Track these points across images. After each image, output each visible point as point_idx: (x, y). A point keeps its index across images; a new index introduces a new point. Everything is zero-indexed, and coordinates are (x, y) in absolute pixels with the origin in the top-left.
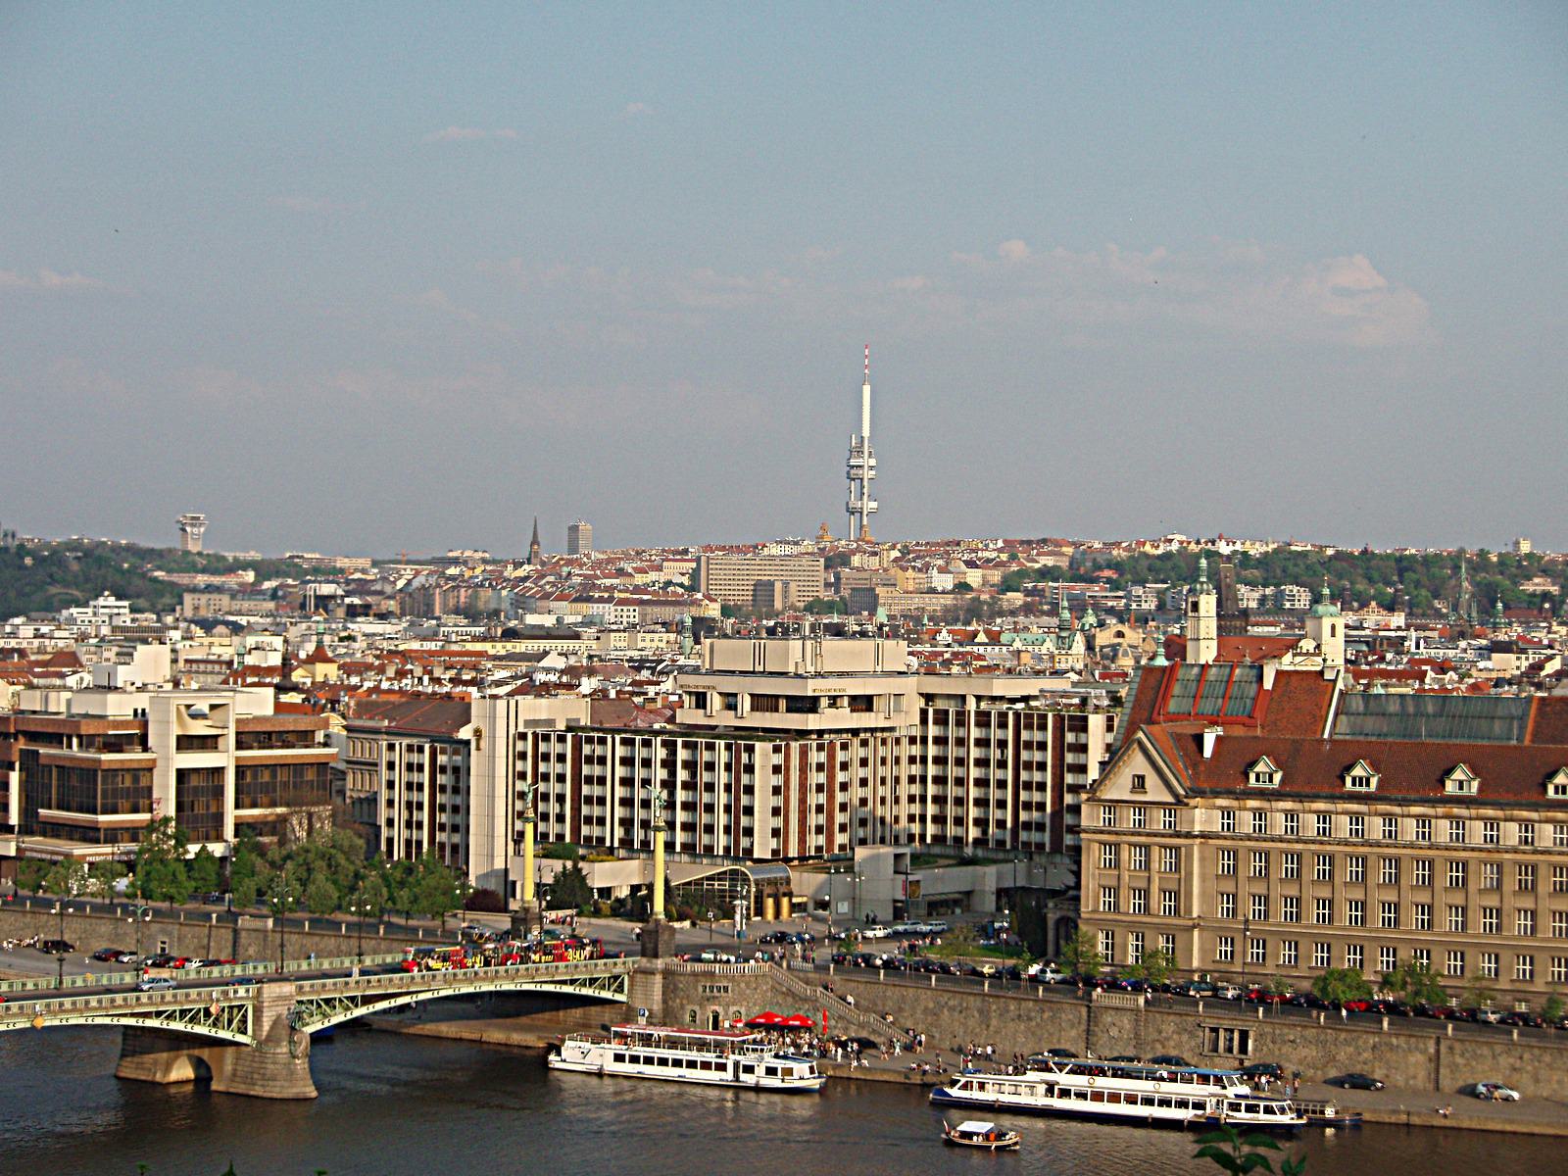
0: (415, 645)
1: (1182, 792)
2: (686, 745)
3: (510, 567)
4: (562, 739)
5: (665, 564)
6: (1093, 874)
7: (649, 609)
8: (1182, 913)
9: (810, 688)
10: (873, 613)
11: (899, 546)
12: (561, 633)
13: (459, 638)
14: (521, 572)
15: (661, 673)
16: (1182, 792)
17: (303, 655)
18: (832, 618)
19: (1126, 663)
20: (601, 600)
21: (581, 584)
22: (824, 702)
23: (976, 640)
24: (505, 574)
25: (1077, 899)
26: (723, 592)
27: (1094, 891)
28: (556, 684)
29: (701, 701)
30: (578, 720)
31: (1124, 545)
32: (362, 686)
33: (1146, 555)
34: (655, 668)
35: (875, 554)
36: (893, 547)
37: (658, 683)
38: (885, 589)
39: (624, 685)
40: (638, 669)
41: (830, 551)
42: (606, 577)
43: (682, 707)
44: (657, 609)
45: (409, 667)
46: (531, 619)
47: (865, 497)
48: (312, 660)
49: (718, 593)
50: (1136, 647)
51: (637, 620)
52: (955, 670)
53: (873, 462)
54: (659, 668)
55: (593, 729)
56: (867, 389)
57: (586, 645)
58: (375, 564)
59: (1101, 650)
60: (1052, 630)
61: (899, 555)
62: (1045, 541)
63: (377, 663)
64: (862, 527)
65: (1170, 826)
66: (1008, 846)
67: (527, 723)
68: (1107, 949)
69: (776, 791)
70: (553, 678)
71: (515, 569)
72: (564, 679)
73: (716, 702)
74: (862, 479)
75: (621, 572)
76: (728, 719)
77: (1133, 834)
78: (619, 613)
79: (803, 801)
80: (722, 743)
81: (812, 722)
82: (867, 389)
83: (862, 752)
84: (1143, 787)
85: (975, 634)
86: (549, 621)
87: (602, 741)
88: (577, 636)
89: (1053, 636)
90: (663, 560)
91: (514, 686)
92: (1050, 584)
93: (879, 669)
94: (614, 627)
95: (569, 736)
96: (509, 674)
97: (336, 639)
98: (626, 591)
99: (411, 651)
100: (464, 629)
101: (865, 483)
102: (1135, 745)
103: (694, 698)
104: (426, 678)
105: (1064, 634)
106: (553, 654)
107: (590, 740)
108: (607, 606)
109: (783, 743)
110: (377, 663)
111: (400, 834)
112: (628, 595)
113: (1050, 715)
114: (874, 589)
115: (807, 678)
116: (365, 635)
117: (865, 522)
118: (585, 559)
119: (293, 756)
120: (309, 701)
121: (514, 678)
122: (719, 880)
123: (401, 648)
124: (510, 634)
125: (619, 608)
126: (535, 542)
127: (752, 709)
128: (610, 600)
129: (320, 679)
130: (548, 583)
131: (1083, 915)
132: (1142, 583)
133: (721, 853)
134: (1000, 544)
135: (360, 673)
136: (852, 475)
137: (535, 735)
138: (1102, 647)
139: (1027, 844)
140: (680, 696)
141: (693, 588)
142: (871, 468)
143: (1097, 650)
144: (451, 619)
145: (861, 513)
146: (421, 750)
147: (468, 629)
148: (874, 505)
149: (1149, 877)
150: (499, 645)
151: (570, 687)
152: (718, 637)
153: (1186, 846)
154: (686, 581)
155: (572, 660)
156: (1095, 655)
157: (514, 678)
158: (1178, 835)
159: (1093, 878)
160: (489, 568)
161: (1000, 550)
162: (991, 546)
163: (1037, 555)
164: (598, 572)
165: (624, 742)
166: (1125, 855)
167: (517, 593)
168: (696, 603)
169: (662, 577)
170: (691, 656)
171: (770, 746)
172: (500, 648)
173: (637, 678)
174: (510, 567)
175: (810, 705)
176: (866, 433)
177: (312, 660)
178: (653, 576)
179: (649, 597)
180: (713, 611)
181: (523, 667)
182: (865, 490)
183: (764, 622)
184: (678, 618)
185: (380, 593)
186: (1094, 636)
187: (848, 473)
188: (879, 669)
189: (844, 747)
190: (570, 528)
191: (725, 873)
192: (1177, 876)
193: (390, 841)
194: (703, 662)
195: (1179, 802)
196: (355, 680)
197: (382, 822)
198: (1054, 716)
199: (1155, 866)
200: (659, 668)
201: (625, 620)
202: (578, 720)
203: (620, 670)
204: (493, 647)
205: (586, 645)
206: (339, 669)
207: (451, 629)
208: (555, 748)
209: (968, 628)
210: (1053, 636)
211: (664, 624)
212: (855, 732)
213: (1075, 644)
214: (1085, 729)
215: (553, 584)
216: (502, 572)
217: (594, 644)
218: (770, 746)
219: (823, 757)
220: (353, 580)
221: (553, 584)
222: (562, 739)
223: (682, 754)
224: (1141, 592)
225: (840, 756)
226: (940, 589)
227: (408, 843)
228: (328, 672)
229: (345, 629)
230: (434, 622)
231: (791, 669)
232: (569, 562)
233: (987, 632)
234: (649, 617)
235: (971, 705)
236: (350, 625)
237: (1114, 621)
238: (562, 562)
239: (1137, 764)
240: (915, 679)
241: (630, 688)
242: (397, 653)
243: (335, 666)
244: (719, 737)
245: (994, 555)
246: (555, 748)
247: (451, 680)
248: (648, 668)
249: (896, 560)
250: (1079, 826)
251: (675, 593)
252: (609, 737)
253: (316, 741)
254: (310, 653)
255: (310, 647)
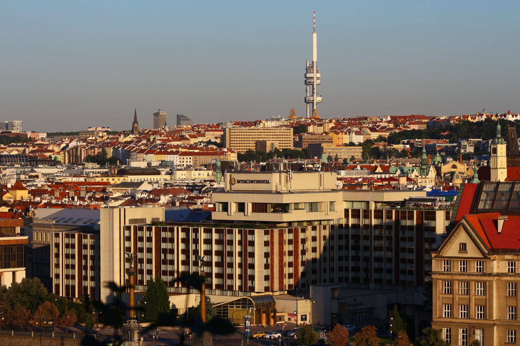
0: (70, 179)
1: (486, 252)
2: (216, 232)
3: (122, 136)
4: (149, 229)
5: (207, 133)
6: (439, 297)
7: (198, 157)
8: (488, 318)
9: (286, 199)
10: (320, 157)
11: (334, 121)
12: (150, 171)
13: (94, 175)
14: (128, 139)
15: (204, 192)
16: (486, 252)
17: (9, 186)
18: (298, 160)
19: (458, 182)
20: (172, 153)
21: (160, 145)
22: (292, 207)
23: (376, 171)
24: (119, 140)
25: (431, 311)
26: (238, 148)
27: (440, 305)
28: (146, 199)
29: (225, 207)
30: (159, 219)
31: (457, 118)
32: (41, 202)
33: (468, 121)
34: (201, 189)
35: (321, 125)
36: (331, 121)
37: (202, 198)
38: (327, 144)
39: (184, 199)
40: (192, 191)
41: (296, 124)
42: (174, 140)
43: (215, 211)
44: (202, 157)
45: (67, 191)
46: (134, 164)
47: (315, 95)
48: (14, 188)
49: (236, 148)
50: (463, 174)
51: (191, 164)
52: (364, 188)
53: (319, 75)
54: (203, 190)
55: (167, 224)
56: (315, 35)
57: (163, 178)
58: (49, 135)
59: (444, 175)
60: (417, 165)
61: (334, 125)
62: (413, 117)
63: (49, 189)
64: (313, 110)
65: (480, 271)
66: (393, 283)
67: (132, 221)
68: (447, 338)
69: (266, 244)
70: (145, 196)
71: (125, 137)
72: (151, 196)
73: (233, 208)
74: (313, 85)
75: (182, 138)
76: (240, 217)
77: (460, 275)
78: (181, 160)
79: (281, 260)
80: (237, 230)
81: (286, 217)
82: (315, 35)
83: (313, 233)
84: (465, 249)
85: (376, 167)
86: (143, 165)
87: (172, 230)
88: (158, 173)
89: (418, 168)
90: (206, 131)
91: (124, 201)
92: (417, 140)
93: (321, 188)
94: (179, 168)
95: (154, 227)
96: (121, 194)
97: (27, 177)
98: (185, 147)
99: (68, 183)
100: (97, 170)
101: (315, 87)
102: (461, 227)
103: (221, 205)
104: (76, 198)
105: (424, 167)
106: (146, 183)
107: (165, 230)
108: (175, 156)
109: (270, 229)
110: (49, 189)
111: (62, 282)
112: (186, 150)
113: (415, 212)
114: (320, 145)
115: (282, 194)
116: (44, 175)
117: (315, 108)
118: (163, 131)
119: (3, 241)
120: (13, 211)
121: (124, 196)
122: (236, 304)
123: (63, 181)
124: (122, 173)
125: (182, 157)
126: (135, 122)
127: (253, 211)
128: (177, 153)
129: (18, 198)
130: (143, 144)
131: (434, 320)
132: (467, 138)
133: (237, 289)
134: (389, 119)
135: (40, 195)
136: (308, 82)
137: (135, 227)
138: (445, 174)
139: (404, 282)
140: (214, 205)
141: (221, 145)
142: (318, 78)
143: (442, 175)
144: (90, 165)
145: (313, 103)
146: (73, 236)
147: (99, 170)
148: (319, 99)
149: (469, 298)
150: (116, 179)
151: (154, 201)
152: (233, 172)
153: (489, 281)
154: (218, 141)
155: (156, 186)
156: (441, 178)
157: (124, 196)
158: (485, 275)
159: (439, 300)
160: (111, 136)
161: (389, 122)
162: (384, 120)
163: (409, 124)
164: (170, 138)
165: (183, 230)
166: (456, 287)
167: (126, 150)
168: (223, 153)
169: (205, 139)
170: (221, 183)
171: (262, 231)
172: (118, 180)
173: (191, 195)
174: (122, 136)
175: (284, 208)
176: (315, 59)
177: (14, 188)
178: (200, 139)
179: (198, 151)
180: (233, 157)
181: (129, 190)
182: (315, 91)
183: (261, 163)
184: (213, 162)
185: (52, 151)
186: (440, 167)
187: (306, 81)
188: (321, 188)
189: (304, 231)
190: (154, 114)
191: (239, 300)
192: (484, 297)
193: (57, 286)
194: (226, 186)
195: (485, 257)
196: (38, 199)
197: (53, 275)
198: (417, 212)
199: (472, 292)
200: (203, 190)
201: (185, 164)
202: (159, 219)
203: (181, 191)
204: (113, 180)
205: (163, 178)
206: (29, 193)
207: (90, 170)
208: (146, 234)
209: (372, 165)
210: (418, 168)
211: (206, 166)
212: (310, 222)
213: (430, 172)
214: (434, 219)
215: (146, 145)
216: (118, 139)
217: (168, 177)
218: (262, 231)
219: (291, 236)
220: (37, 144)
221: (146, 145)
222: (149, 229)
223: (192, 236)
224: (466, 143)
225: (301, 236)
226: (357, 143)
227: (67, 286)
228: (23, 195)
229: (32, 171)
230: (81, 167)
231: (274, 189)
232: (155, 133)
233: (382, 167)
234: (198, 162)
235: (372, 207)
236: (35, 169)
237: (451, 160)
238: (150, 133)
239: (462, 237)
240: (341, 194)
241: (187, 201)
242: (61, 183)
243: (27, 191)
244: (235, 227)
245: (386, 124)
246: (146, 234)
247: (90, 198)
248: (197, 190)
249: (332, 128)
250: (431, 271)
251: (212, 149)
252: (175, 228)
253: (16, 232)
254: (13, 185)
255: (13, 182)
